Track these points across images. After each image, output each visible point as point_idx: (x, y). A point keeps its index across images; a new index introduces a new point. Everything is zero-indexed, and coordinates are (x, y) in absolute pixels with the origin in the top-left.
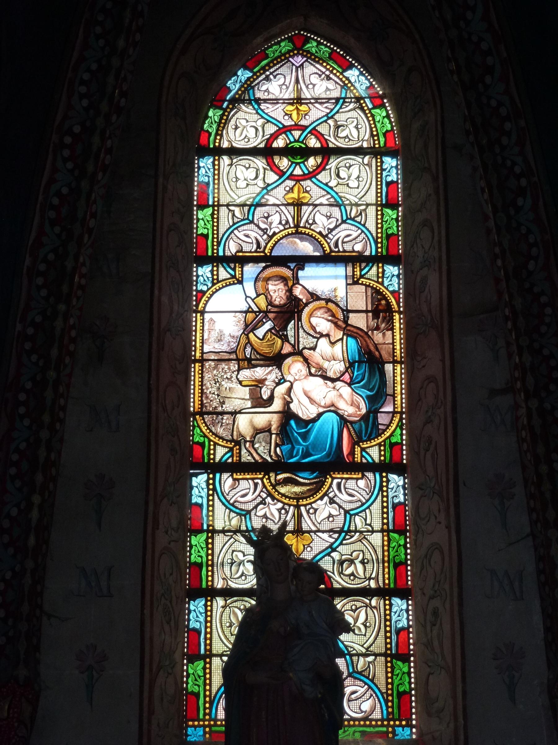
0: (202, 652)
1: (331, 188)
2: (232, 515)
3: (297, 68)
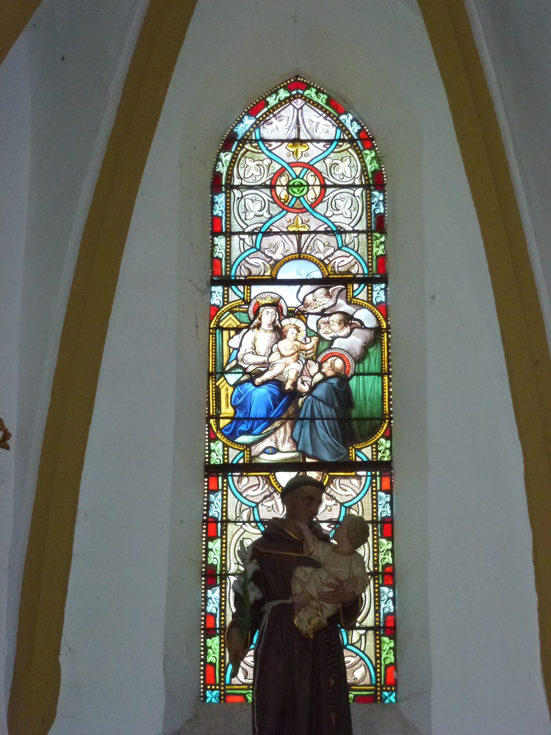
0: (224, 230)
1: (327, 218)
2: (244, 507)
3: (298, 110)
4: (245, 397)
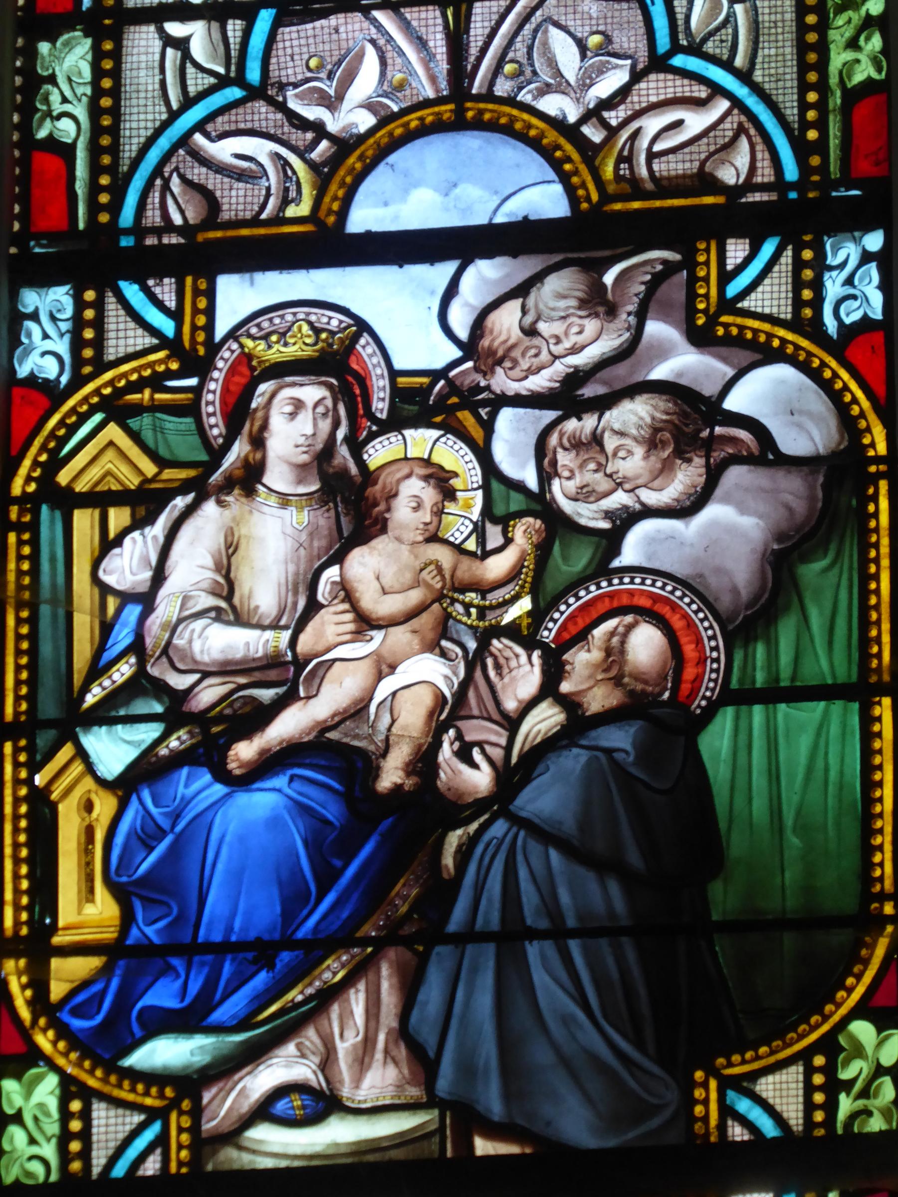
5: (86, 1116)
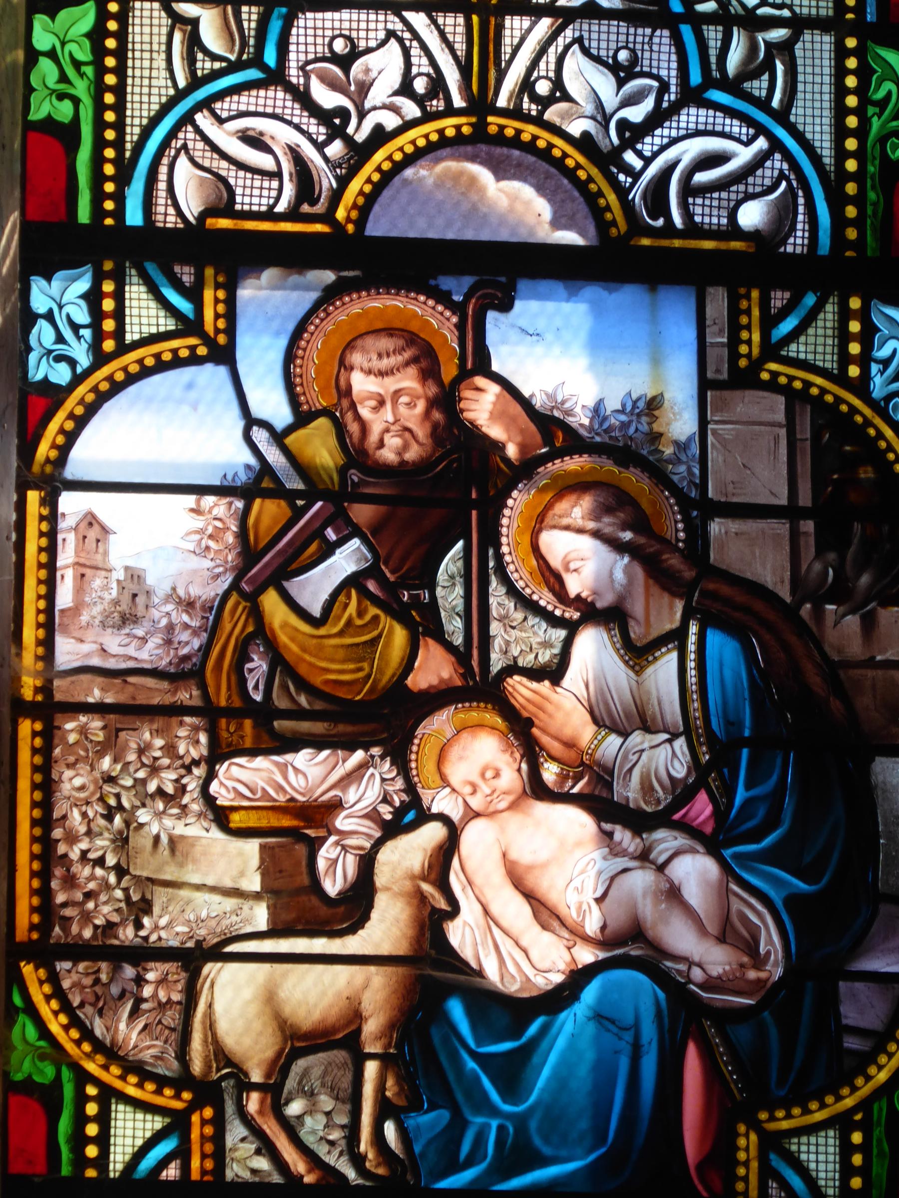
4: (374, 681)
5: (845, 359)
